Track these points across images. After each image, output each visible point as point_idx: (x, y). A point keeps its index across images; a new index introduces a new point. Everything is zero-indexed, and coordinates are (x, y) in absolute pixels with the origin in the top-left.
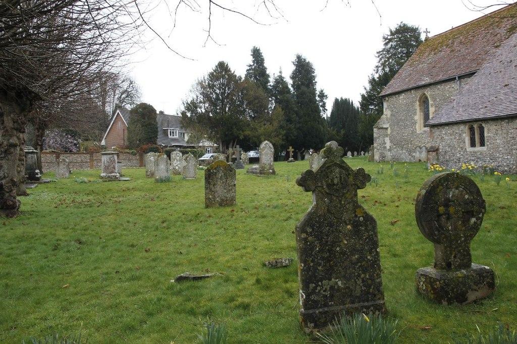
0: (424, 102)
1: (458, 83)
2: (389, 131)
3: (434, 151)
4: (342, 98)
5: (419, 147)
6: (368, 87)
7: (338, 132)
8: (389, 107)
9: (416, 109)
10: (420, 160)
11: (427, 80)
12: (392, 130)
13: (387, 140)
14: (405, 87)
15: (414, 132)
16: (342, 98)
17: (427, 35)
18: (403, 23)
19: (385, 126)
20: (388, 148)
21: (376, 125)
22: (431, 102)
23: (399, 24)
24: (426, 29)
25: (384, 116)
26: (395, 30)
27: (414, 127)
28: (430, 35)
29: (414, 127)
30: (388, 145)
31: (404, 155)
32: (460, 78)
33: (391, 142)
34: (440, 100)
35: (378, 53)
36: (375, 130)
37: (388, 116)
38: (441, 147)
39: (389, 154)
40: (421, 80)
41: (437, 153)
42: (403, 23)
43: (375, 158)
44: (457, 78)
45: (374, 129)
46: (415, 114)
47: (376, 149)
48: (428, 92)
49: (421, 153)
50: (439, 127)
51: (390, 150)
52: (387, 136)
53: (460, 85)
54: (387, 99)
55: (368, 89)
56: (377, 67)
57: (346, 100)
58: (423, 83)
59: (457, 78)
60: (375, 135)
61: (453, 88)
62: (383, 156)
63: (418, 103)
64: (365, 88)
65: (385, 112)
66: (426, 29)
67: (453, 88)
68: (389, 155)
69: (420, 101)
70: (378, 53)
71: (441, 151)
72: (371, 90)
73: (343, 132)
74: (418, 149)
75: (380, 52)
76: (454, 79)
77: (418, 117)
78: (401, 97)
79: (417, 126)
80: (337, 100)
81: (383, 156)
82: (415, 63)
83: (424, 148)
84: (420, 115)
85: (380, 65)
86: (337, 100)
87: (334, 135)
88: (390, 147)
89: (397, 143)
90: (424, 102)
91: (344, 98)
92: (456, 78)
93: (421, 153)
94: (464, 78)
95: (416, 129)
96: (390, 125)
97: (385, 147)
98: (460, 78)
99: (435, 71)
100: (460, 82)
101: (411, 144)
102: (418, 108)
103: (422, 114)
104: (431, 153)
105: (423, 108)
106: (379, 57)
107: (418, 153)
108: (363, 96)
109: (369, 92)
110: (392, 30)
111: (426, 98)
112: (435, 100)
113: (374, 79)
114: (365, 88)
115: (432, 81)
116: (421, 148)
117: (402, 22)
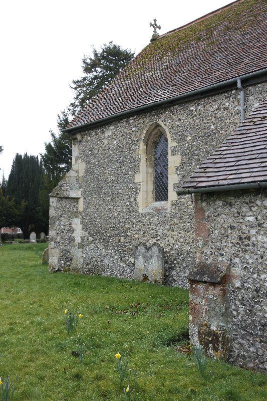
0: (156, 140)
1: (241, 96)
2: (81, 205)
3: (213, 284)
4: (26, 155)
5: (145, 245)
6: (58, 133)
7: (18, 203)
8: (82, 153)
9: (139, 160)
10: (145, 278)
11: (162, 95)
12: (88, 205)
13: (77, 223)
14: (120, 111)
15: (132, 209)
16: (26, 155)
17: (155, 32)
18: (113, 43)
19: (73, 194)
20: (78, 240)
21: (55, 191)
22: (171, 144)
23: (108, 45)
24: (155, 20)
25: (71, 173)
26: (101, 51)
27: (132, 199)
28: (161, 32)
29: (132, 199)
30: (79, 234)
31: (112, 263)
32: (246, 82)
33: (85, 228)
34: (194, 138)
35: (74, 82)
36: (53, 201)
37: (82, 173)
38: (237, 271)
39: (80, 254)
40: (150, 95)
41: (224, 291)
42: (113, 43)
43: (50, 261)
44: (239, 85)
45: (51, 200)
46: (136, 169)
47: (53, 243)
48: (166, 121)
49: (147, 259)
50: (232, 199)
51: (81, 246)
52: (76, 214)
53: (52, 273)
54: (79, 137)
55: (57, 136)
56: (73, 105)
57: (32, 157)
58: (158, 99)
59: (239, 85)
60: (52, 213)
61: (226, 109)
62: (66, 257)
63: (142, 146)
64: (53, 135)
65: (75, 166)
66: (155, 20)
67: (226, 109)
68: (79, 257)
69: (146, 142)
70: (74, 82)
71: (238, 284)
72: (61, 138)
73: (24, 203)
74: (142, 249)
75: (78, 82)
76: (230, 87)
77: (143, 177)
78: (108, 134)
79: (140, 198)
80: (18, 158)
81: (66, 257)
82: (135, 73)
83: (155, 250)
84: (147, 173)
85: (77, 102)
86: (18, 158)
87: (10, 207)
88: (82, 238)
89: (95, 232)
90: (156, 140)
91: (29, 155)
92: (235, 83)
93: (147, 259)
94: (255, 84)
95: (137, 204)
96: (83, 193)
97: (72, 239)
98: (246, 82)
99: (178, 79)
100: (246, 95)
101: (126, 237)
102: (143, 157)
103: (150, 170)
104: (201, 287)
105: (153, 159)
106: (76, 89)
107: (141, 258)
108: (49, 147)
109: (59, 141)
110: (98, 52)
111: (161, 134)
112: (181, 138)
113: (66, 120)
114: (53, 135)
115: (177, 95)
116: (148, 249)
117: (111, 42)
